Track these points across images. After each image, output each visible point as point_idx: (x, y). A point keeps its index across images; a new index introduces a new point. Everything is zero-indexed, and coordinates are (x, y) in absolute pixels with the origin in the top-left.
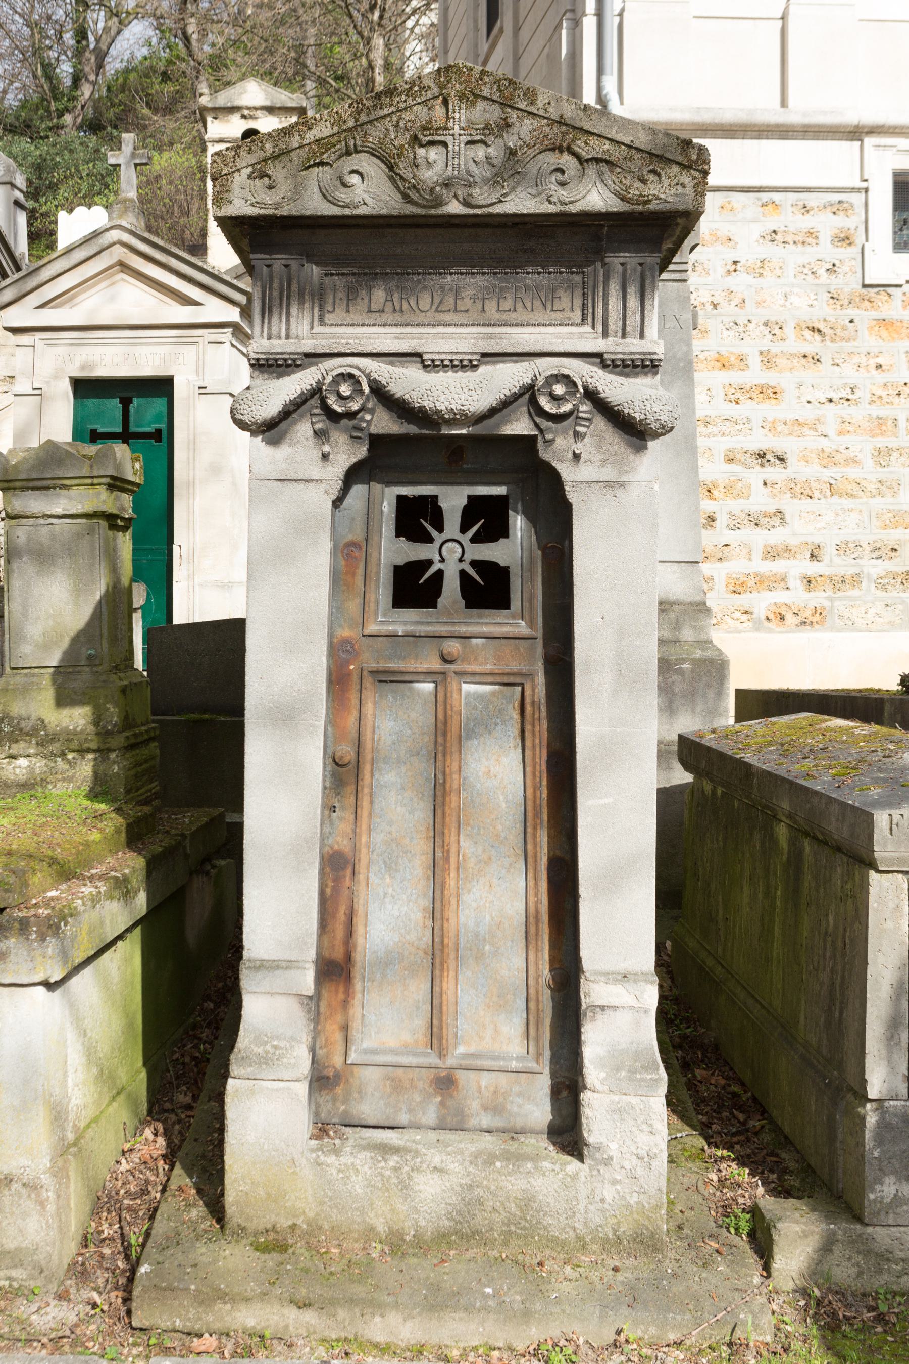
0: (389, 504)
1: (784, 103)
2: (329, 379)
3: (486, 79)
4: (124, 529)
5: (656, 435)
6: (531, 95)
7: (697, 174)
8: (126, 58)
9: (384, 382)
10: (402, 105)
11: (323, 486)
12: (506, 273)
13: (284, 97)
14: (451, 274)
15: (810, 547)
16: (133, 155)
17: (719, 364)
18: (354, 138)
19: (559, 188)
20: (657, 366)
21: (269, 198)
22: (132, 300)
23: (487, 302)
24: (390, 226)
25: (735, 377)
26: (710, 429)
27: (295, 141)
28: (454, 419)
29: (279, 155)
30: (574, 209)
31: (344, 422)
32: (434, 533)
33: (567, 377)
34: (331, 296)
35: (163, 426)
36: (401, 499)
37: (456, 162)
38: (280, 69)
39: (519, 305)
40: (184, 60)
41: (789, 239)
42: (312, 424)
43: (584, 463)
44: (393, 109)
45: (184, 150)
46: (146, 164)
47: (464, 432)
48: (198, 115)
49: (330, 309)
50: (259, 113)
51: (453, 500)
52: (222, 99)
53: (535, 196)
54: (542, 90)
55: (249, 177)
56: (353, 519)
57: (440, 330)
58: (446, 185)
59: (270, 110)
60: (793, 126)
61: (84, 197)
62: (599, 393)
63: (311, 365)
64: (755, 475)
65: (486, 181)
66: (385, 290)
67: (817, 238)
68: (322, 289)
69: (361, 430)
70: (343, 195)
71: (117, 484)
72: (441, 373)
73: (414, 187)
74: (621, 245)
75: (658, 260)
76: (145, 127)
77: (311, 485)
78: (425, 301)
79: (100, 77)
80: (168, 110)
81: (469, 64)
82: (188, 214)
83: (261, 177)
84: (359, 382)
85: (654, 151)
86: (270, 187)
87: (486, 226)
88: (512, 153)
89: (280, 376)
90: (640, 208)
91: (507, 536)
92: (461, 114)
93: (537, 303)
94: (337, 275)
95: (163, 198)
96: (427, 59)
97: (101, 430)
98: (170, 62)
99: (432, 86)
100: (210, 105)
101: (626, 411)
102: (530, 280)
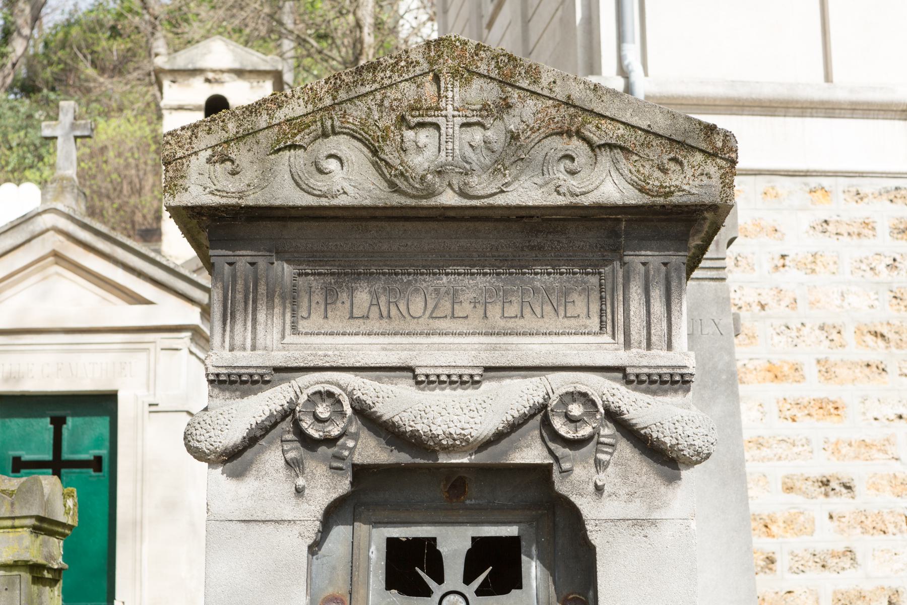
0: (378, 550)
1: (828, 78)
2: (303, 398)
3: (482, 54)
4: (53, 582)
5: (690, 464)
6: (534, 73)
7: (723, 163)
8: (67, 9)
9: (369, 402)
10: (387, 82)
11: (297, 529)
12: (511, 274)
13: (255, 59)
14: (447, 274)
15: (888, 593)
16: (73, 127)
17: (771, 375)
18: (331, 118)
19: (568, 177)
20: (688, 382)
21: (232, 185)
22: (69, 298)
23: (489, 306)
24: (374, 218)
25: (789, 390)
26: (765, 452)
27: (263, 121)
28: (454, 446)
29: (244, 137)
30: (586, 201)
31: (323, 449)
32: (432, 584)
33: (585, 395)
34: (306, 300)
35: (104, 452)
36: (392, 543)
37: (450, 146)
38: (252, 25)
39: (527, 310)
40: (137, 13)
41: (843, 229)
42: (283, 451)
43: (606, 495)
44: (376, 86)
45: (135, 116)
46: (89, 137)
47: (466, 460)
48: (153, 78)
49: (305, 314)
50: (226, 77)
51: (454, 543)
52: (182, 60)
53: (541, 186)
54: (546, 67)
55: (209, 161)
56: (334, 568)
57: (436, 339)
58: (439, 172)
59: (240, 73)
60: (840, 103)
61: (13, 171)
62: (622, 414)
63: (282, 381)
64: (818, 506)
65: (485, 169)
66: (370, 292)
67: (874, 229)
68: (294, 291)
69: (343, 459)
70: (319, 183)
71: (44, 526)
72: (437, 391)
73: (402, 174)
74: (643, 242)
75: (685, 260)
76: (89, 90)
77: (283, 527)
78: (417, 305)
79: (35, 31)
80: (118, 70)
81: (462, 38)
82: (139, 192)
83: (223, 162)
84: (339, 402)
85: (674, 137)
86: (234, 173)
87: (487, 219)
88: (514, 137)
89: (244, 394)
90: (661, 200)
91: (520, 587)
92: (455, 94)
93: (548, 308)
94: (312, 274)
95: (109, 174)
96: (424, 17)
97: (26, 457)
98: (120, 15)
99: (421, 61)
100: (167, 67)
101: (655, 435)
102: (540, 281)
